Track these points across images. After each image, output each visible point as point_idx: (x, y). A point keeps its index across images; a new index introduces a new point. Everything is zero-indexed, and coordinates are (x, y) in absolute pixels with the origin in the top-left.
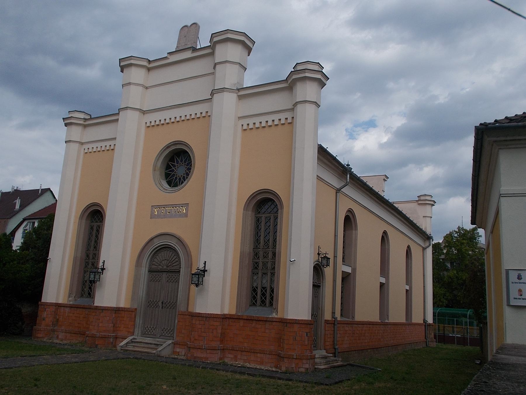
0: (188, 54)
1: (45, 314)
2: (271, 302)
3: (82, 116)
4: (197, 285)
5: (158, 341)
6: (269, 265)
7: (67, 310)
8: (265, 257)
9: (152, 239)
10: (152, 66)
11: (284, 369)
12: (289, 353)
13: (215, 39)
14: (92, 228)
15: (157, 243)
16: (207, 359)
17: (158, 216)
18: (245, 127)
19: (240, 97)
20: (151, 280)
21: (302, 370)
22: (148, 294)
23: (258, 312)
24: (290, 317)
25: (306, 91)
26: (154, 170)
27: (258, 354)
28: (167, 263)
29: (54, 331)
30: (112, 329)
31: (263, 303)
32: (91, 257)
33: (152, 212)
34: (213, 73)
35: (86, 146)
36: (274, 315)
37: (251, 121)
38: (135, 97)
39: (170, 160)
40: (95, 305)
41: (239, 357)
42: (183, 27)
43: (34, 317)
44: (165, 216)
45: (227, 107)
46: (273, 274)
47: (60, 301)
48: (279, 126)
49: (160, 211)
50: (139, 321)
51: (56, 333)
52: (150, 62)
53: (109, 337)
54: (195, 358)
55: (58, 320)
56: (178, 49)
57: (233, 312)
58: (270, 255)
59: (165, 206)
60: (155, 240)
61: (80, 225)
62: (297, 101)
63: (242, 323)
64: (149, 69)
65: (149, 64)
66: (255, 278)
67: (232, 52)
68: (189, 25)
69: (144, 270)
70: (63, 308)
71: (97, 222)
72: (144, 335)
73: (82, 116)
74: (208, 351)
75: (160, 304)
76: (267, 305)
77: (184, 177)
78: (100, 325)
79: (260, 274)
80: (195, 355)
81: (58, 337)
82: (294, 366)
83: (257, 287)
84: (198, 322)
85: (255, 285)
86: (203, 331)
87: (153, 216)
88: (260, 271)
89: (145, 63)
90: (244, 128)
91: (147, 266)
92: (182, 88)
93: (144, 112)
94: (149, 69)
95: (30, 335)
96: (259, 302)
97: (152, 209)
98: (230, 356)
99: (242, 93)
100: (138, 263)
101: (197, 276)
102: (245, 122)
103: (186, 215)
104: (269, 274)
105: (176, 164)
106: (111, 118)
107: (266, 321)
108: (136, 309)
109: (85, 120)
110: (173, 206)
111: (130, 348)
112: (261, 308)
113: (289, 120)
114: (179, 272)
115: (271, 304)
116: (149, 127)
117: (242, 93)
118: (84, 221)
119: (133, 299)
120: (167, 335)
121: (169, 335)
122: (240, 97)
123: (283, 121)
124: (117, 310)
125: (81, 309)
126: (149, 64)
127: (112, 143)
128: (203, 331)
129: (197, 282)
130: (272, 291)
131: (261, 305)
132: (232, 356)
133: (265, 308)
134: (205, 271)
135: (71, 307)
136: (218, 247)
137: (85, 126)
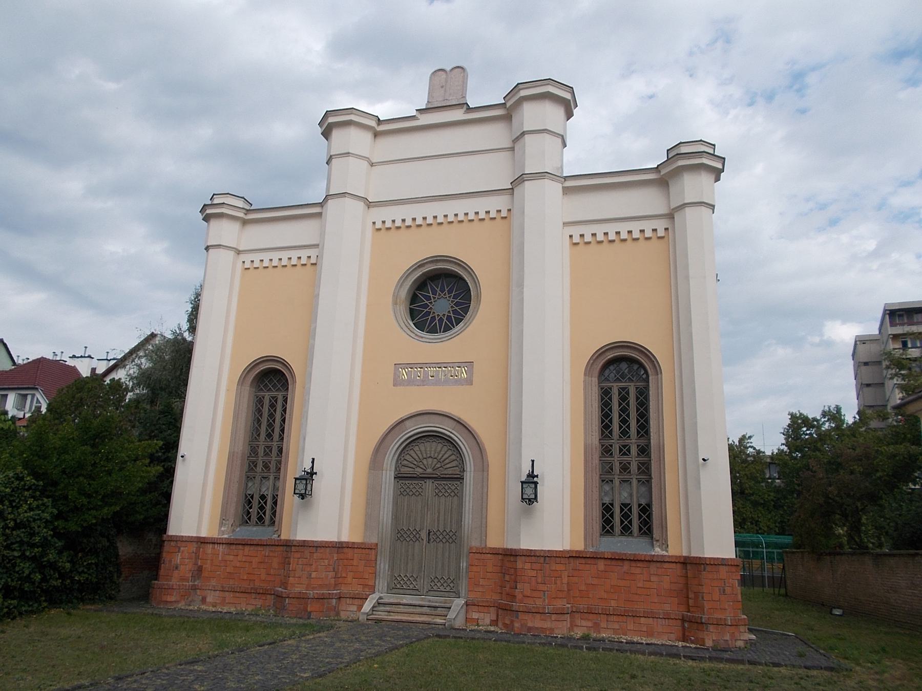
0: (458, 115)
1: (178, 559)
2: (272, 519)
3: (240, 203)
4: (302, 496)
5: (430, 601)
6: (272, 466)
7: (221, 548)
8: (266, 454)
9: (402, 421)
10: (381, 129)
11: (709, 643)
12: (716, 616)
13: (331, 120)
14: (260, 401)
15: (413, 428)
16: (552, 630)
17: (410, 382)
18: (576, 239)
19: (567, 191)
20: (400, 494)
21: (740, 644)
22: (396, 517)
23: (633, 546)
24: (707, 555)
25: (693, 186)
26: (395, 303)
27: (642, 619)
28: (429, 463)
29: (194, 588)
30: (333, 581)
31: (626, 530)
32: (261, 451)
33: (470, 373)
34: (512, 149)
35: (243, 257)
36: (658, 551)
37: (588, 231)
38: (352, 176)
39: (417, 289)
40: (283, 537)
41: (603, 625)
42: (458, 67)
43: (152, 564)
44: (424, 383)
45: (545, 207)
46: (277, 478)
47: (204, 534)
48: (652, 240)
49: (408, 373)
50: (383, 566)
51: (198, 592)
52: (380, 122)
53: (330, 597)
54: (530, 629)
55: (200, 569)
56: (430, 106)
57: (580, 546)
58: (275, 451)
59: (422, 366)
60: (407, 423)
61: (239, 394)
62: (686, 201)
63: (601, 565)
64: (376, 135)
65: (378, 125)
66: (250, 484)
67: (550, 114)
68: (448, 69)
69: (388, 476)
70: (211, 545)
71: (270, 390)
72: (394, 591)
73: (240, 203)
74: (554, 617)
75: (424, 535)
76: (267, 522)
77: (449, 318)
78: (314, 575)
79: (258, 478)
80: (530, 624)
81: (204, 600)
82: (727, 637)
83: (612, 505)
84: (527, 566)
85: (607, 500)
86: (539, 580)
87: (397, 382)
88: (616, 477)
89: (373, 123)
90: (574, 241)
91: (393, 468)
92: (467, 166)
93: (369, 204)
94: (376, 135)
95: (144, 596)
96: (254, 517)
97: (396, 370)
98: (584, 623)
99: (569, 183)
100: (376, 461)
101: (304, 482)
102: (576, 231)
103: (469, 382)
104: (272, 477)
105: (438, 295)
106: (314, 212)
107: (651, 561)
108: (377, 544)
109: (248, 211)
110: (439, 365)
111: (382, 615)
112: (623, 538)
113: (313, 260)
114: (461, 479)
115: (273, 523)
116: (379, 230)
117: (569, 183)
118: (247, 388)
119: (367, 526)
120: (442, 588)
121: (448, 589)
122: (567, 191)
123: (303, 261)
124: (340, 547)
125: (252, 548)
126: (378, 125)
127: (313, 253)
128: (539, 580)
129: (303, 492)
130: (275, 503)
131: (622, 534)
132: (590, 624)
133: (630, 539)
134: (312, 474)
135: (229, 543)
136: (547, 434)
137: (245, 222)
